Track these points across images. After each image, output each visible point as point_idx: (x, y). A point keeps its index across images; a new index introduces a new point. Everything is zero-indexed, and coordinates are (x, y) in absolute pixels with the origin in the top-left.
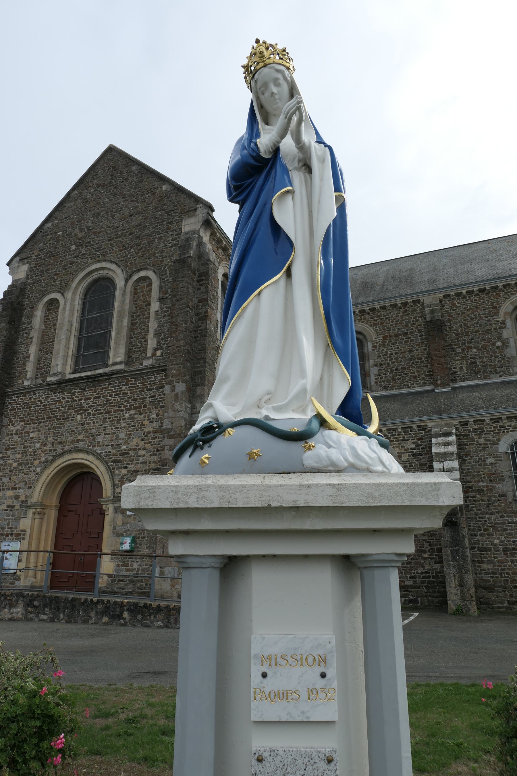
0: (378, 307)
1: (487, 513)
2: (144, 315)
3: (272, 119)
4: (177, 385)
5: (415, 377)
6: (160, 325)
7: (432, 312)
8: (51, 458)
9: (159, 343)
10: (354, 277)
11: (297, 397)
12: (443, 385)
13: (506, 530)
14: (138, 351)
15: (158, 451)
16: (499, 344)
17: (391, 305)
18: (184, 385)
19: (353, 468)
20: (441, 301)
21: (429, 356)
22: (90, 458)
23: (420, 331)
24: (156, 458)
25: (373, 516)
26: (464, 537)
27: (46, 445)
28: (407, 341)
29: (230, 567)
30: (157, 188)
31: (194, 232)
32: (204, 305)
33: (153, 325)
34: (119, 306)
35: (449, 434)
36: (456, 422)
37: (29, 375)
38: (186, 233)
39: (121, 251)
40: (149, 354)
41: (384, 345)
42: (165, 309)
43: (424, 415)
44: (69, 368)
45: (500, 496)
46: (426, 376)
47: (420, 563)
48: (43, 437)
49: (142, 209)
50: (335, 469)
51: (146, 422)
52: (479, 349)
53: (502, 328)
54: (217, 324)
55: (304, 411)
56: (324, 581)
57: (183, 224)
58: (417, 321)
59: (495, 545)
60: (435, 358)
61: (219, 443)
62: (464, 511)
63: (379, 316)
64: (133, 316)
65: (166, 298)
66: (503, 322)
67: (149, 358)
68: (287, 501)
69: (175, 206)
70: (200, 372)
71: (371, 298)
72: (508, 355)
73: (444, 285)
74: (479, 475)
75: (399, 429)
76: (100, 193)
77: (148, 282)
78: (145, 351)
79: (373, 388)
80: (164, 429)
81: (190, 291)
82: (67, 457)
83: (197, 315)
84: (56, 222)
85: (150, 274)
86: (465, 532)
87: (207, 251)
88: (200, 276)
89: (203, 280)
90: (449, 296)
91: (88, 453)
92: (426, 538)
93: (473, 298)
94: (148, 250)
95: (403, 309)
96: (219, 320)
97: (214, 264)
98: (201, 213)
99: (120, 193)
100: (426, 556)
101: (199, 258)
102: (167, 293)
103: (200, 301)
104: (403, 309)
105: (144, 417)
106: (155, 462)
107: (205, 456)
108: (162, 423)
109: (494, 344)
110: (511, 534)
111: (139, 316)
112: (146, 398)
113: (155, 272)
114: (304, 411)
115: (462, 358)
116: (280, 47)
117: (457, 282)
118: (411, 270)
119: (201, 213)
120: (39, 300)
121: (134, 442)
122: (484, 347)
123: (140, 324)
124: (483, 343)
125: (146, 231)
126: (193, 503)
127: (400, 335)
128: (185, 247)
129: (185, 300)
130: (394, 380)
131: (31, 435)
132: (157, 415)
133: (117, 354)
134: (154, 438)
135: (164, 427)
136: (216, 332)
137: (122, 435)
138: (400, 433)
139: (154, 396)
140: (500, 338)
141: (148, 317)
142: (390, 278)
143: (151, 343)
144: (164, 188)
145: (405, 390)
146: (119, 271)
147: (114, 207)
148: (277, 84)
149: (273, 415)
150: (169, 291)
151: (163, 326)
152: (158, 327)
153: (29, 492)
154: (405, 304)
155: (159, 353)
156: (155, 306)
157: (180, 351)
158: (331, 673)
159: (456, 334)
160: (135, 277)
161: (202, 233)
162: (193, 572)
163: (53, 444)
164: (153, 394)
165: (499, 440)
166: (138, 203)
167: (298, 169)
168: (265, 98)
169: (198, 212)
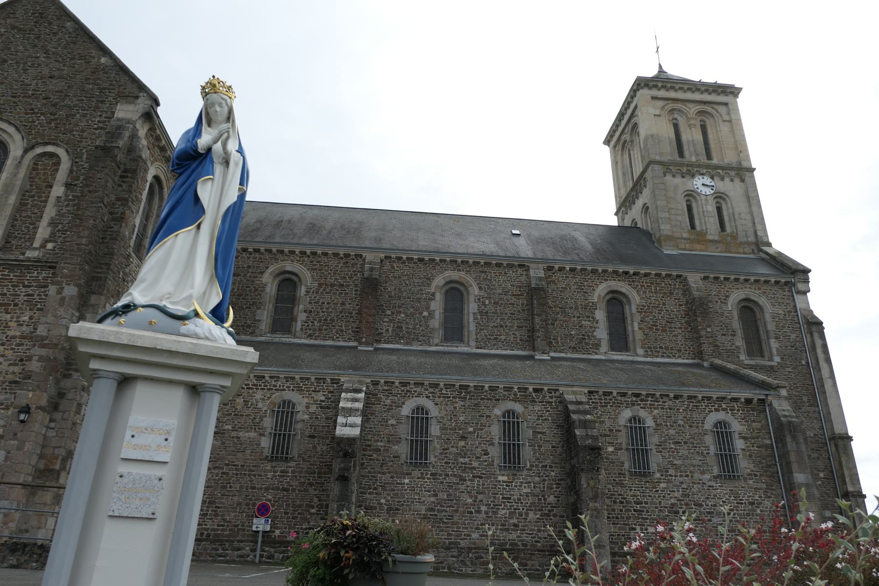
0: (319, 252)
1: (379, 473)
2: (40, 197)
3: (213, 124)
4: (66, 287)
5: (342, 331)
6: (60, 214)
7: (371, 269)
9: (53, 234)
10: (304, 215)
11: (185, 299)
12: (367, 344)
13: (394, 490)
14: (21, 238)
15: (21, 360)
16: (425, 314)
17: (333, 254)
18: (76, 289)
19: (207, 338)
20: (382, 261)
21: (360, 312)
23: (356, 286)
24: (17, 369)
25: (212, 364)
26: (352, 492)
28: (340, 293)
29: (125, 382)
30: (93, 58)
31: (129, 121)
32: (122, 205)
33: (50, 212)
34: (7, 178)
35: (358, 391)
36: (368, 381)
38: (118, 120)
39: (27, 114)
40: (36, 244)
41: (317, 292)
42: (71, 197)
43: (340, 369)
45: (394, 457)
46: (353, 331)
47: (306, 518)
49: (68, 75)
50: (197, 337)
51: (12, 324)
52: (407, 315)
53: (430, 299)
54: (134, 230)
55: (189, 308)
56: (178, 396)
57: (118, 108)
58: (356, 275)
59: (381, 504)
60: (365, 315)
61: (131, 315)
62: (358, 468)
63: (319, 262)
64: (24, 195)
65: (75, 185)
66: (433, 294)
67: (36, 249)
68: (166, 347)
69: (111, 85)
70: (100, 279)
71: (315, 242)
72: (431, 326)
73: (388, 246)
74: (378, 435)
75: (313, 379)
76: (14, 37)
77: (54, 160)
78: (32, 239)
79: (298, 334)
80: (37, 336)
81: (109, 185)
83: (111, 213)
85: (61, 152)
86: (355, 487)
87: (141, 146)
88: (125, 171)
89: (127, 177)
90: (390, 257)
92: (317, 492)
93: (412, 265)
94: (64, 124)
95: (344, 260)
96: (137, 225)
97: (145, 163)
98: (142, 104)
99: (42, 46)
100: (313, 511)
101: (128, 151)
102: (78, 179)
103: (118, 199)
104: (344, 260)
105: (12, 318)
106: (14, 373)
107: (122, 320)
108: (36, 329)
109: (421, 313)
110: (397, 494)
111: (33, 197)
112: (19, 295)
113: (67, 151)
114: (189, 308)
115: (390, 321)
116: (228, 84)
117: (401, 246)
118: (361, 223)
119: (142, 104)
122: (412, 314)
123: (32, 206)
124: (412, 310)
125: (67, 102)
126: (112, 339)
127: (336, 285)
128: (115, 133)
129: (100, 193)
130: (320, 330)
132: (31, 318)
134: (18, 345)
135: (38, 333)
136: (130, 238)
138: (312, 384)
139: (33, 295)
141: (46, 201)
142: (339, 226)
143: (43, 231)
144: (103, 60)
145: (330, 343)
146: (17, 137)
147: (30, 59)
148: (220, 105)
149: (169, 306)
150: (82, 178)
151: (63, 216)
152: (56, 215)
154: (347, 256)
155: (50, 246)
156: (58, 190)
157: (79, 250)
158: (171, 439)
159: (390, 297)
160: (39, 150)
161: (138, 126)
162: (102, 380)
164: (31, 292)
165: (403, 403)
166: (64, 65)
167: (221, 164)
168: (211, 111)
169: (139, 101)
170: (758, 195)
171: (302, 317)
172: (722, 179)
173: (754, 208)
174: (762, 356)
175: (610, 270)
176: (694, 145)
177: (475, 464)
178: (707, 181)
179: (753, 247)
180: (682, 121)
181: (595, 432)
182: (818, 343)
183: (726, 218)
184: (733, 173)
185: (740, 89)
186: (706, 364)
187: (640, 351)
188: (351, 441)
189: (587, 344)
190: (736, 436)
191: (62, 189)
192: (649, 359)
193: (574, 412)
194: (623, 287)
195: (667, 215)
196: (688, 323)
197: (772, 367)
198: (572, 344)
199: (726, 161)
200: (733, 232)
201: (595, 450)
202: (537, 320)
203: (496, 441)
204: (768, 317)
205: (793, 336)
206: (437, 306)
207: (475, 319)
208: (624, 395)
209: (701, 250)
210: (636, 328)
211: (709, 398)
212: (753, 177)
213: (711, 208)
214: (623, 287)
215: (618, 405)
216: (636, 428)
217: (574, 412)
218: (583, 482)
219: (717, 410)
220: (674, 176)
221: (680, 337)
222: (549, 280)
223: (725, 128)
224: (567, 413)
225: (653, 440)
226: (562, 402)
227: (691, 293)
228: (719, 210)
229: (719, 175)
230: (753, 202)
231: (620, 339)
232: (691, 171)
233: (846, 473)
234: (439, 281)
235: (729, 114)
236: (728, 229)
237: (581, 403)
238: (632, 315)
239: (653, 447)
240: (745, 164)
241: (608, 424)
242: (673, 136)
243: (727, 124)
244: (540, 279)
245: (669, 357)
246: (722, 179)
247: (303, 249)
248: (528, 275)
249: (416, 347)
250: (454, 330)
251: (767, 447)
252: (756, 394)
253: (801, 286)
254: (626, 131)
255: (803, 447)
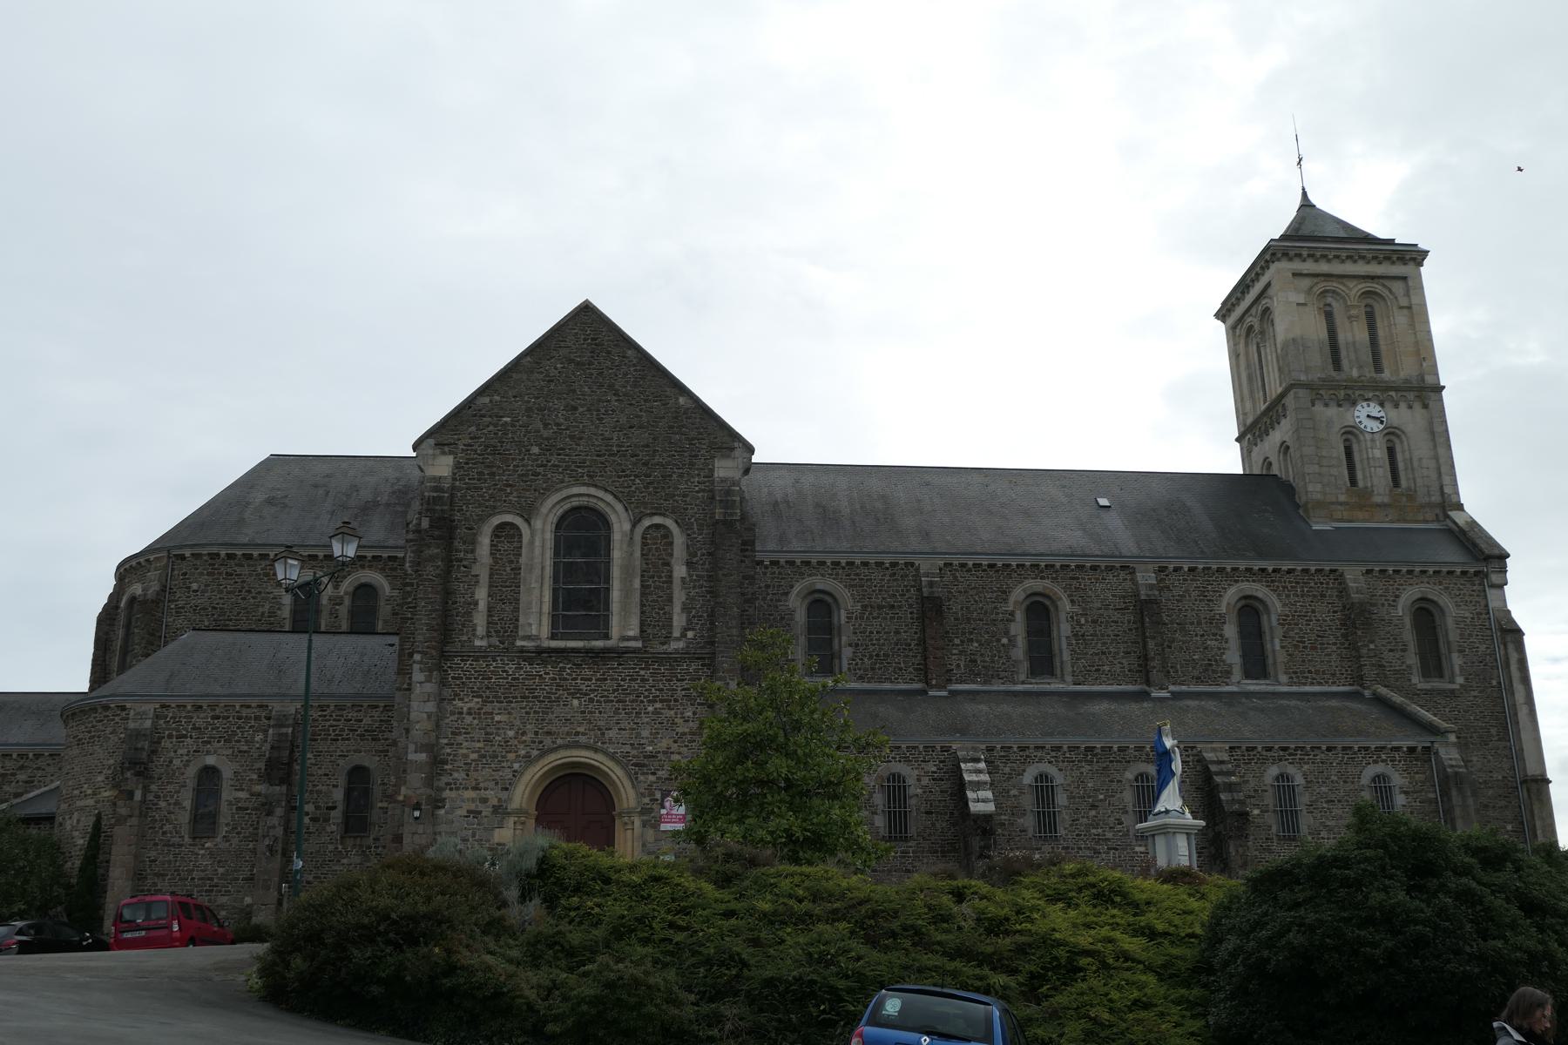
0: (858, 562)
8: (535, 753)
9: (689, 621)
16: (1005, 641)
22: (600, 757)
23: (911, 606)
27: (524, 733)
33: (679, 596)
35: (978, 760)
37: (481, 630)
40: (676, 634)
44: (545, 631)
48: (518, 722)
66: (1012, 614)
82: (563, 753)
84: (497, 398)
91: (596, 750)
109: (999, 640)
120: (482, 519)
121: (663, 744)
131: (497, 718)
133: (623, 626)
137: (645, 733)
140: (1007, 633)
144: (682, 400)
153: (504, 795)
154: (894, 565)
156: (680, 571)
160: (647, 522)
163: (536, 733)
170: (1447, 431)
171: (847, 652)
172: (1396, 406)
173: (1441, 451)
174: (1441, 676)
175: (1242, 568)
176: (1356, 351)
177: (1109, 835)
178: (1375, 410)
179: (1438, 511)
180: (1337, 307)
181: (1241, 796)
182: (1514, 657)
183: (1401, 466)
184: (1411, 396)
185: (1425, 253)
186: (1367, 693)
187: (1283, 678)
188: (987, 817)
189: (1214, 672)
190: (1397, 790)
191: (684, 568)
192: (1294, 689)
193: (1218, 774)
194: (1259, 590)
195: (1316, 468)
196: (1345, 636)
197: (1452, 691)
198: (1196, 673)
199: (1402, 375)
200: (1409, 489)
201: (1243, 816)
202: (1151, 644)
203: (1130, 808)
204: (1450, 622)
205: (1483, 648)
206: (1018, 628)
207: (1069, 644)
208: (1269, 749)
209: (1364, 521)
210: (1278, 647)
211: (1367, 749)
212: (1441, 400)
213: (1379, 453)
214: (1259, 590)
215: (1263, 761)
216: (1284, 786)
217: (1218, 774)
218: (1232, 849)
219: (1375, 762)
220: (1326, 405)
221: (1334, 656)
222: (1161, 587)
223: (1401, 319)
224: (1207, 776)
225: (1303, 799)
226: (1201, 760)
227: (1348, 596)
228: (1391, 452)
229: (1391, 399)
230: (1440, 440)
231: (1256, 664)
232: (1349, 395)
233: (1538, 824)
234: (1018, 594)
235: (1407, 294)
236: (1404, 483)
237: (1222, 762)
238: (1271, 628)
239: (1304, 808)
240: (1429, 379)
241: (1252, 783)
242: (1324, 335)
243: (1405, 311)
244: (1151, 587)
245: (1320, 684)
246: (1396, 406)
247: (836, 557)
248: (1134, 581)
249: (997, 687)
250: (1043, 662)
251: (1430, 801)
252: (1419, 741)
253: (1495, 578)
254: (1253, 311)
255: (1470, 801)
